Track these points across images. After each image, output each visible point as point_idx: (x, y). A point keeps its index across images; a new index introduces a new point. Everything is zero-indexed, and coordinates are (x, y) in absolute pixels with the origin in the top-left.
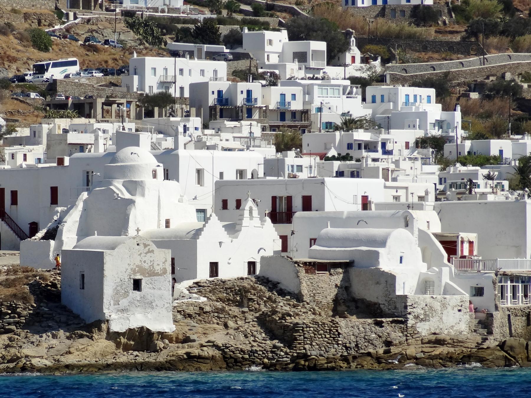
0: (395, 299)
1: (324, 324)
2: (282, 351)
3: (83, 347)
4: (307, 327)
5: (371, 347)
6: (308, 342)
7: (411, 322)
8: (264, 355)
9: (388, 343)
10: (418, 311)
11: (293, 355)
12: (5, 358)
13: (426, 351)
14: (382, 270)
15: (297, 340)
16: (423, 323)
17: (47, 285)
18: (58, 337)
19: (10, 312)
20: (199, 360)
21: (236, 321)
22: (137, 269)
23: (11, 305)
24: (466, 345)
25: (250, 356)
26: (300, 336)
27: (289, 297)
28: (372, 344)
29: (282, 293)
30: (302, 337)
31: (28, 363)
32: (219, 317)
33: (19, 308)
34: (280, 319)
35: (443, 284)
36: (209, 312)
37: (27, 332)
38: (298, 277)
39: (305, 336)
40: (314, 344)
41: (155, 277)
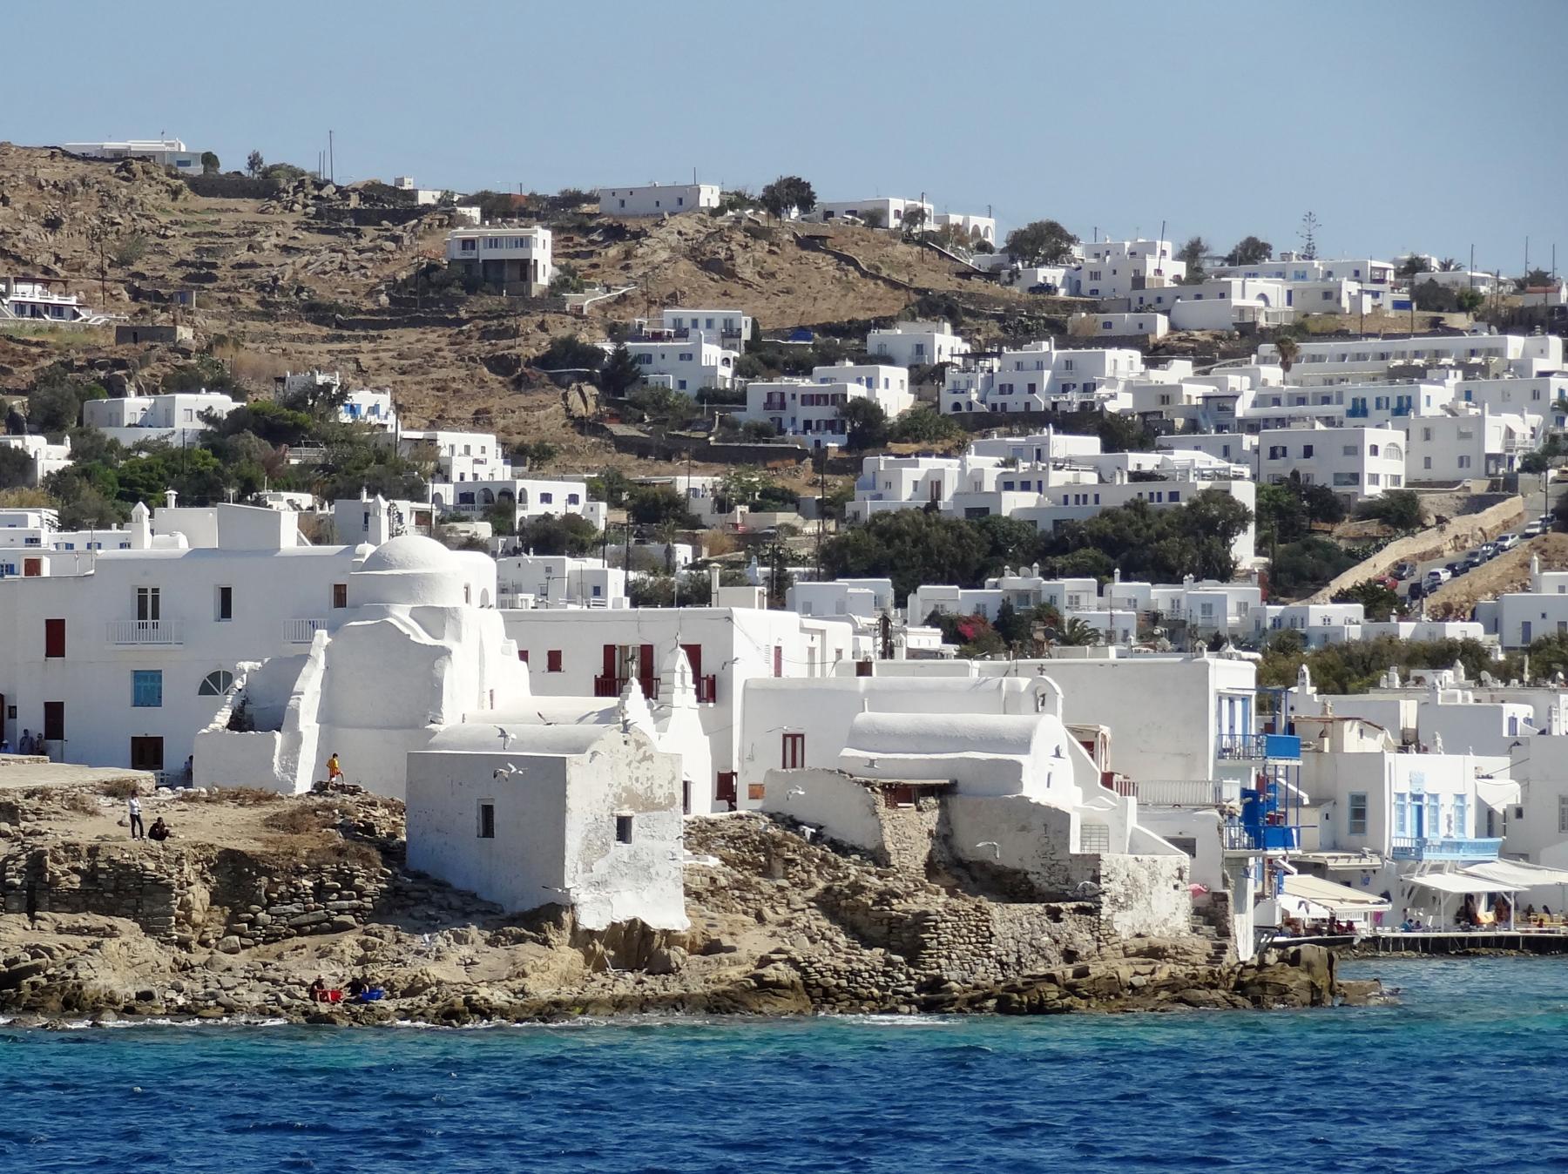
2: (900, 970)
5: (1041, 962)
6: (945, 953)
7: (1106, 910)
8: (872, 980)
9: (1070, 956)
14: (1032, 801)
15: (927, 948)
16: (1124, 912)
20: (778, 991)
22: (624, 795)
23: (341, 871)
25: (849, 982)
26: (932, 939)
27: (857, 857)
28: (1044, 957)
30: (935, 942)
32: (745, 900)
33: (358, 877)
34: (875, 903)
35: (1129, 832)
36: (723, 888)
37: (396, 929)
40: (954, 956)
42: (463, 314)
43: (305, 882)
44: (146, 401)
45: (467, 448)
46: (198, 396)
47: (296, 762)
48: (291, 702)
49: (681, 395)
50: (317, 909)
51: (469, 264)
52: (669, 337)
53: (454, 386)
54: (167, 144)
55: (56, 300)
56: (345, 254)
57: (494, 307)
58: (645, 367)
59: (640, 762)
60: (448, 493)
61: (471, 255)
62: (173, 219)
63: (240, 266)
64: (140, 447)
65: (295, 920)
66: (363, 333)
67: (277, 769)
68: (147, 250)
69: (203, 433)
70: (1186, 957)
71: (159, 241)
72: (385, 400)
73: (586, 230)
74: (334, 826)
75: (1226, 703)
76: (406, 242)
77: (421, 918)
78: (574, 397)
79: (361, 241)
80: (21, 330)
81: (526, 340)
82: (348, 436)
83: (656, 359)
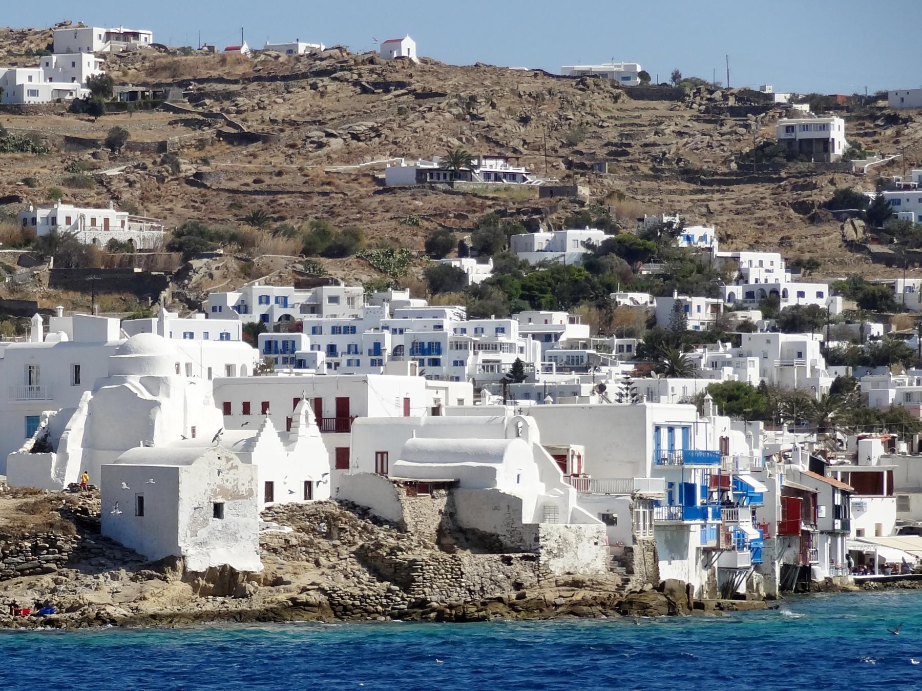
0: (521, 530)
1: (445, 561)
2: (397, 595)
3: (159, 591)
4: (426, 565)
5: (498, 590)
6: (428, 584)
7: (543, 558)
8: (377, 601)
9: (518, 586)
10: (551, 544)
11: (410, 601)
12: (62, 605)
13: (565, 596)
14: (501, 492)
15: (416, 582)
16: (557, 559)
17: (77, 511)
18: (120, 578)
19: (48, 546)
21: (328, 557)
22: (218, 490)
23: (49, 537)
24: (606, 588)
25: (361, 602)
26: (419, 576)
27: (387, 527)
28: (500, 587)
29: (378, 521)
30: (421, 578)
31: (102, 612)
32: (308, 553)
33: (59, 540)
34: (388, 554)
35: (570, 510)
36: (295, 546)
37: (77, 572)
38: (399, 500)
39: (426, 576)
40: (434, 586)
41: (239, 500)
42: (783, 174)
43: (26, 544)
44: (550, 235)
45: (761, 263)
46: (582, 231)
47: (64, 471)
48: (63, 435)
49: (919, 225)
50: (33, 560)
51: (790, 142)
52: (914, 188)
53: (770, 221)
54: (616, 66)
55: (511, 170)
56: (711, 136)
57: (804, 170)
58: (896, 207)
59: (229, 470)
60: (738, 291)
61: (792, 136)
62: (610, 115)
63: (646, 145)
64: (541, 264)
65: (20, 567)
66: (717, 188)
67: (53, 475)
68: (587, 135)
69: (585, 255)
70: (600, 587)
71: (598, 129)
72: (710, 231)
73: (873, 118)
74: (57, 510)
75: (664, 432)
76: (753, 127)
77: (95, 565)
78: (848, 228)
79: (723, 128)
80: (485, 191)
81: (821, 191)
82: (681, 257)
83: (903, 202)
